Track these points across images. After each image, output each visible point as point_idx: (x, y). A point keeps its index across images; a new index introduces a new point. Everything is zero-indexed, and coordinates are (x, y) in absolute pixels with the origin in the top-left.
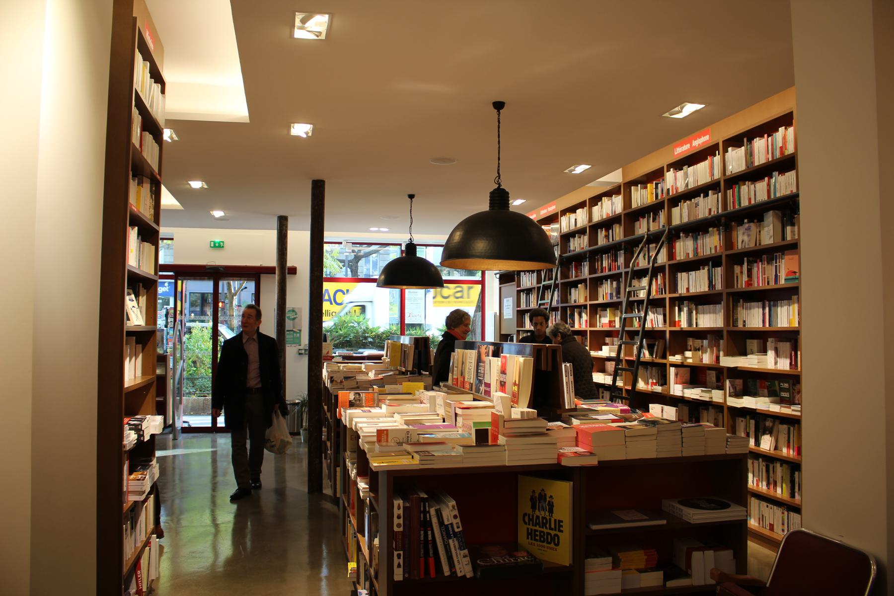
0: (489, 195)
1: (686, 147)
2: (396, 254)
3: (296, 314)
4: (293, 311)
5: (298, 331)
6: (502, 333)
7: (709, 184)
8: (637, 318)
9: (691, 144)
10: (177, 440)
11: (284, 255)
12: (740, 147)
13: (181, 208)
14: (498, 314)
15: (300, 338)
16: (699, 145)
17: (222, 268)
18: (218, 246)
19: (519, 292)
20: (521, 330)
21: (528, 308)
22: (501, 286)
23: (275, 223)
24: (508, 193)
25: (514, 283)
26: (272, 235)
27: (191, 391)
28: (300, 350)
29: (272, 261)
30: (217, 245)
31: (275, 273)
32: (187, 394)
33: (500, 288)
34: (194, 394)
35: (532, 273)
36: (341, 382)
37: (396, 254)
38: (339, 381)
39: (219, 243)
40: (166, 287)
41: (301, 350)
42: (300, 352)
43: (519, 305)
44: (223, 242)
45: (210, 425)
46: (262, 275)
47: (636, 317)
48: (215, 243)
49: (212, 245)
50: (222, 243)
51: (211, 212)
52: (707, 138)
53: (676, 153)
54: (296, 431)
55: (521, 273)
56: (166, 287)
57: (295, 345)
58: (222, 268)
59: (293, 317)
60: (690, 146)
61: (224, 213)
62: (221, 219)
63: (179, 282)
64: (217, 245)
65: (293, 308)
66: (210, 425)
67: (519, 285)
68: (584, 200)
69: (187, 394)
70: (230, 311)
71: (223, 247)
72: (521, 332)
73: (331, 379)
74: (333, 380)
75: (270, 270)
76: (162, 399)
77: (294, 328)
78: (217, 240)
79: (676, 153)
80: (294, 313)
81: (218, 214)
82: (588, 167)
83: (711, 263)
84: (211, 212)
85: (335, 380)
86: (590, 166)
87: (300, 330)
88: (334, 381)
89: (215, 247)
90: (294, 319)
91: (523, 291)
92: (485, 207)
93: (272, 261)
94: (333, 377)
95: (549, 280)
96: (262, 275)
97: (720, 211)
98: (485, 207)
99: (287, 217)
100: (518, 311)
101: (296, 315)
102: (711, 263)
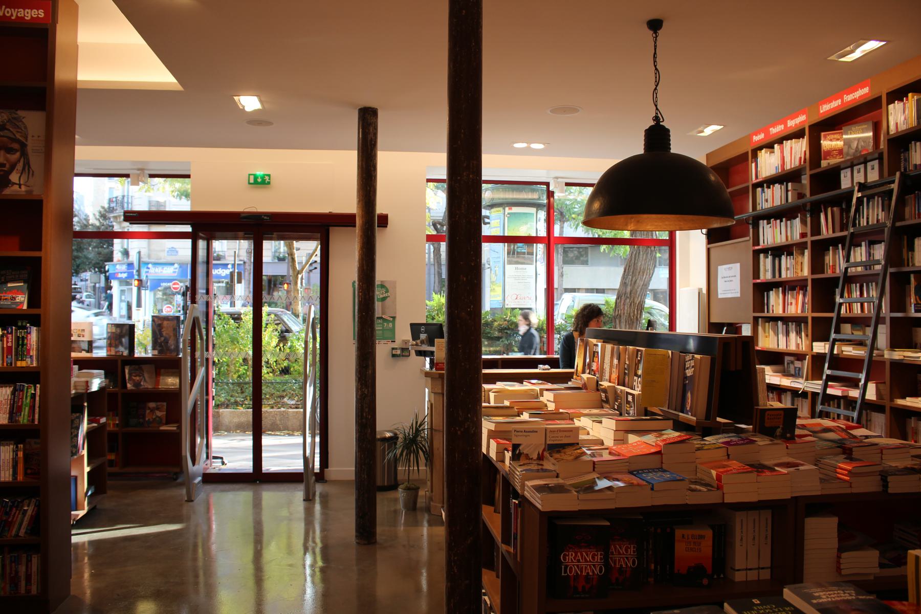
0: (644, 134)
1: (836, 104)
2: (499, 220)
3: (387, 291)
4: (382, 286)
5: (391, 319)
6: (713, 320)
7: (774, 176)
8: (847, 304)
9: (786, 124)
10: (192, 501)
11: (371, 180)
12: (803, 137)
13: (180, 88)
14: (705, 291)
15: (393, 330)
16: (796, 125)
17: (268, 216)
18: (261, 183)
19: (756, 254)
20: (762, 317)
21: (777, 279)
22: (710, 246)
23: (352, 133)
24: (668, 131)
25: (747, 238)
26: (349, 160)
27: (238, 399)
28: (393, 349)
29: (349, 204)
30: (259, 180)
31: (355, 226)
32: (232, 404)
33: (708, 250)
34: (242, 405)
35: (787, 220)
36: (541, 458)
37: (499, 220)
38: (535, 456)
39: (263, 178)
40: (229, 269)
41: (396, 349)
42: (394, 353)
43: (756, 274)
44: (269, 176)
45: (251, 470)
46: (331, 228)
47: (846, 303)
48: (256, 178)
49: (252, 181)
50: (267, 178)
51: (236, 98)
52: (866, 90)
53: (821, 112)
54: (386, 484)
55: (761, 222)
56: (229, 269)
57: (385, 341)
58: (268, 216)
59: (382, 296)
60: (787, 123)
61: (261, 101)
62: (255, 120)
63: (202, 244)
64: (259, 180)
65: (382, 281)
66: (251, 470)
67: (756, 241)
68: (745, 151)
69: (232, 404)
70: (294, 292)
71: (269, 183)
72: (760, 319)
73: (514, 451)
74: (520, 454)
75: (346, 220)
76: (175, 428)
77: (383, 313)
78: (260, 173)
79: (821, 112)
80: (384, 290)
81: (250, 103)
82: (718, 128)
83: (785, 253)
84: (236, 98)
85: (525, 452)
86: (722, 127)
87: (394, 318)
88: (522, 457)
89: (256, 182)
90: (384, 299)
91: (765, 251)
92: (638, 149)
93: (349, 204)
94: (519, 445)
95: (841, 230)
96: (331, 228)
97: (783, 203)
98: (638, 149)
99: (377, 109)
100: (755, 284)
101: (386, 292)
102: (785, 253)
